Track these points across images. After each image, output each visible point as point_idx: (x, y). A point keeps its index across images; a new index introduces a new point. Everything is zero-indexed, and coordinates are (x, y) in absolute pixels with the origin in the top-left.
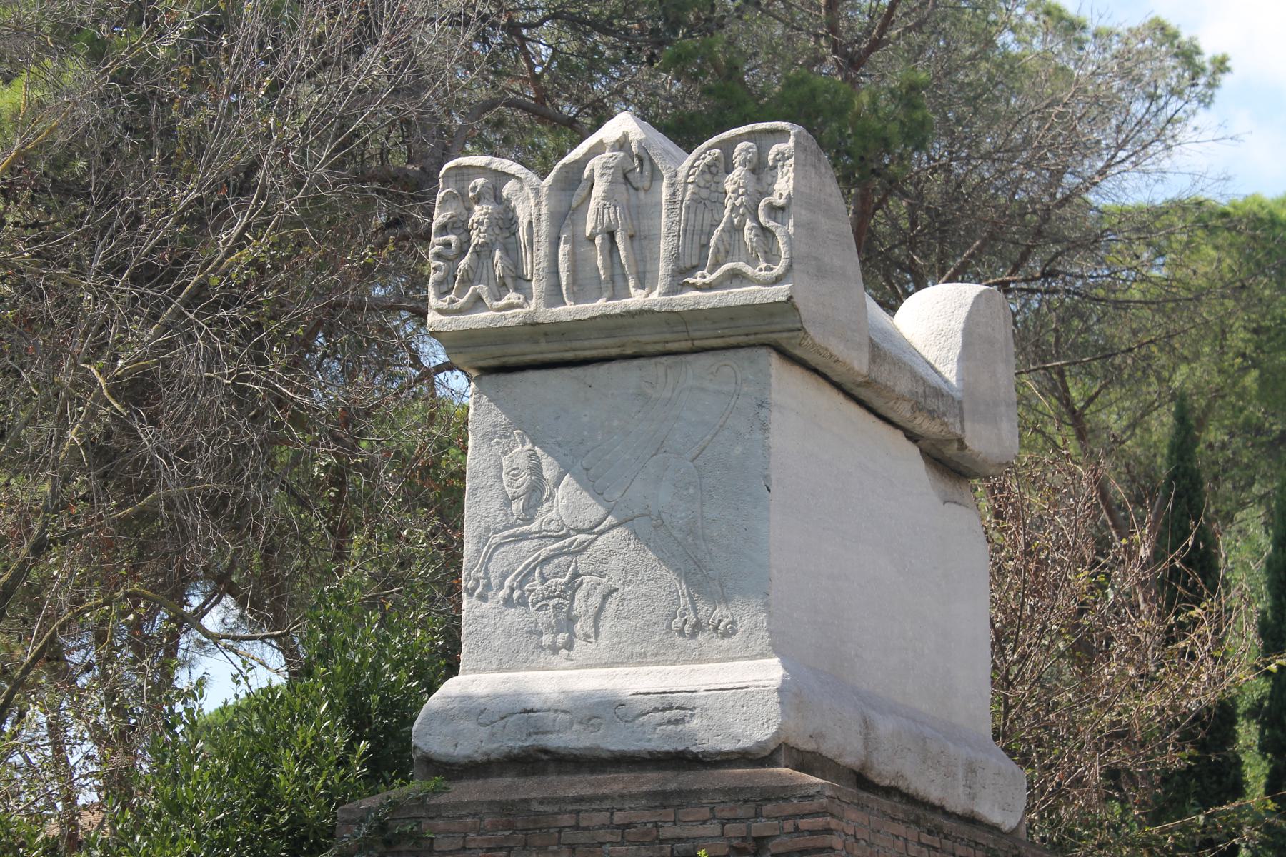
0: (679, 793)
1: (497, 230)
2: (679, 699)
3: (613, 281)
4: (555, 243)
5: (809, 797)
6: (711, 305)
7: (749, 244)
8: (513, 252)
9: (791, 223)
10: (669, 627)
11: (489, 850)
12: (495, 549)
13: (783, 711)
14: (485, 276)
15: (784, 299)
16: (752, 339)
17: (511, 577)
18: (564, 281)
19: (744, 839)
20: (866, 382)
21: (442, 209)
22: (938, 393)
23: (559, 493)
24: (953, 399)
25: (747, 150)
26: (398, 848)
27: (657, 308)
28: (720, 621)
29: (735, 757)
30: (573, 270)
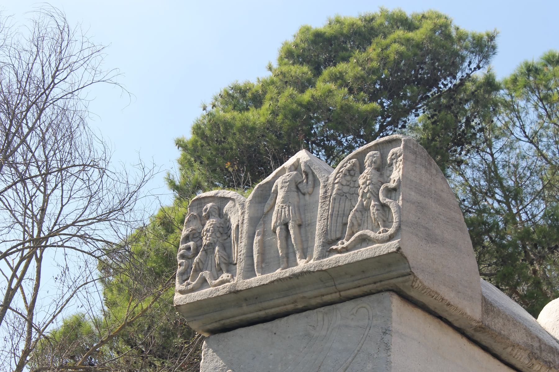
1: (218, 235)
3: (288, 258)
4: (251, 238)
6: (346, 262)
7: (373, 217)
8: (226, 248)
9: (401, 198)
14: (210, 265)
15: (395, 250)
16: (378, 286)
20: (480, 327)
21: (187, 226)
25: (373, 156)
27: (312, 269)
30: (263, 253)
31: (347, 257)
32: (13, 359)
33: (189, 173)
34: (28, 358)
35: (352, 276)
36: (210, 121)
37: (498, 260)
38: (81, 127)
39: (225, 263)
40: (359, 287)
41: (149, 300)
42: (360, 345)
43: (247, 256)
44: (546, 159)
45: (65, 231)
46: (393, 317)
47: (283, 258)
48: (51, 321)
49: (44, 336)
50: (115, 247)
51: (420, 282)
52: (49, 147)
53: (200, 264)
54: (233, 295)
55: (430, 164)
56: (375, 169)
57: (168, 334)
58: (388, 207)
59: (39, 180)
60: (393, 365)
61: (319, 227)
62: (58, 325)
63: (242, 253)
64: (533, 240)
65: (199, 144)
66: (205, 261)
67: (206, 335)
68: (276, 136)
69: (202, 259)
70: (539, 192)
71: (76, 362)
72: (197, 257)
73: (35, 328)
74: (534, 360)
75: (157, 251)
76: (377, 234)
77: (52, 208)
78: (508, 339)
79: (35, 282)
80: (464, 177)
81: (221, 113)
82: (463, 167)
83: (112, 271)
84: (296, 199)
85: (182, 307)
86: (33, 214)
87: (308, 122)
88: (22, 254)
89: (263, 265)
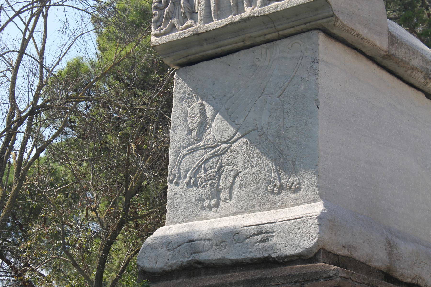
2: (266, 227)
5: (330, 278)
6: (283, 8)
10: (266, 190)
12: (183, 157)
13: (321, 230)
14: (177, 14)
17: (190, 171)
20: (387, 55)
23: (214, 124)
27: (256, 15)
28: (293, 184)
29: (295, 258)
31: (283, 4)
32: (30, 93)
34: (42, 92)
35: (288, 19)
37: (401, 7)
39: (189, 12)
40: (293, 27)
41: (131, 45)
42: (295, 72)
43: (206, 6)
46: (320, 49)
47: (234, 6)
48: (58, 63)
49: (52, 74)
50: (103, 4)
51: (341, 22)
53: (170, 13)
54: (196, 37)
57: (148, 71)
60: (320, 86)
62: (63, 66)
63: (202, 3)
66: (174, 11)
67: (176, 68)
69: (171, 10)
72: (167, 8)
73: (45, 69)
75: (136, 7)
78: (408, 64)
79: (43, 33)
85: (157, 47)
88: (32, 12)
89: (219, 13)
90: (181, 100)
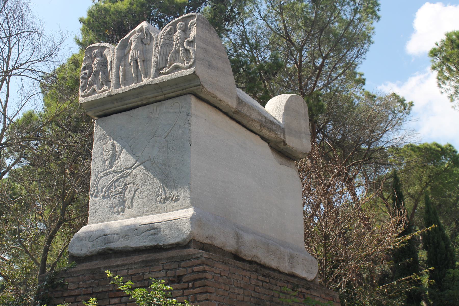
0: (152, 261)
1: (101, 66)
4: (118, 68)
5: (197, 258)
8: (106, 73)
10: (156, 200)
11: (86, 288)
12: (100, 179)
13: (192, 226)
15: (192, 73)
18: (121, 80)
19: (174, 277)
20: (236, 111)
22: (272, 123)
23: (121, 156)
24: (280, 127)
25: (181, 24)
26: (57, 289)
27: (150, 83)
28: (174, 196)
29: (175, 246)
30: (124, 75)
31: (168, 77)
33: (87, 36)
34: (5, 134)
35: (171, 86)
36: (97, 8)
38: (28, 11)
43: (116, 77)
44: (271, 29)
45: (21, 67)
48: (16, 114)
50: (48, 75)
52: (10, 22)
54: (109, 98)
55: (210, 28)
56: (182, 31)
57: (78, 120)
58: (189, 51)
59: (6, 40)
61: (153, 61)
62: (20, 116)
64: (264, 70)
65: (91, 20)
67: (96, 118)
68: (132, 16)
70: (267, 46)
71: (31, 135)
74: (262, 128)
75: (71, 77)
76: (183, 65)
77: (14, 55)
78: (250, 117)
79: (6, 94)
80: (230, 39)
81: (102, 4)
82: (229, 33)
83: (47, 88)
84: (141, 47)
86: (3, 58)
87: (149, 9)
90: (99, 140)
